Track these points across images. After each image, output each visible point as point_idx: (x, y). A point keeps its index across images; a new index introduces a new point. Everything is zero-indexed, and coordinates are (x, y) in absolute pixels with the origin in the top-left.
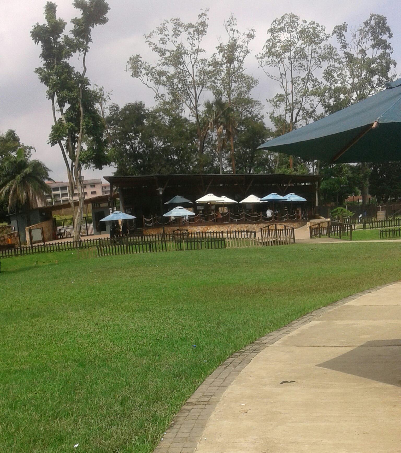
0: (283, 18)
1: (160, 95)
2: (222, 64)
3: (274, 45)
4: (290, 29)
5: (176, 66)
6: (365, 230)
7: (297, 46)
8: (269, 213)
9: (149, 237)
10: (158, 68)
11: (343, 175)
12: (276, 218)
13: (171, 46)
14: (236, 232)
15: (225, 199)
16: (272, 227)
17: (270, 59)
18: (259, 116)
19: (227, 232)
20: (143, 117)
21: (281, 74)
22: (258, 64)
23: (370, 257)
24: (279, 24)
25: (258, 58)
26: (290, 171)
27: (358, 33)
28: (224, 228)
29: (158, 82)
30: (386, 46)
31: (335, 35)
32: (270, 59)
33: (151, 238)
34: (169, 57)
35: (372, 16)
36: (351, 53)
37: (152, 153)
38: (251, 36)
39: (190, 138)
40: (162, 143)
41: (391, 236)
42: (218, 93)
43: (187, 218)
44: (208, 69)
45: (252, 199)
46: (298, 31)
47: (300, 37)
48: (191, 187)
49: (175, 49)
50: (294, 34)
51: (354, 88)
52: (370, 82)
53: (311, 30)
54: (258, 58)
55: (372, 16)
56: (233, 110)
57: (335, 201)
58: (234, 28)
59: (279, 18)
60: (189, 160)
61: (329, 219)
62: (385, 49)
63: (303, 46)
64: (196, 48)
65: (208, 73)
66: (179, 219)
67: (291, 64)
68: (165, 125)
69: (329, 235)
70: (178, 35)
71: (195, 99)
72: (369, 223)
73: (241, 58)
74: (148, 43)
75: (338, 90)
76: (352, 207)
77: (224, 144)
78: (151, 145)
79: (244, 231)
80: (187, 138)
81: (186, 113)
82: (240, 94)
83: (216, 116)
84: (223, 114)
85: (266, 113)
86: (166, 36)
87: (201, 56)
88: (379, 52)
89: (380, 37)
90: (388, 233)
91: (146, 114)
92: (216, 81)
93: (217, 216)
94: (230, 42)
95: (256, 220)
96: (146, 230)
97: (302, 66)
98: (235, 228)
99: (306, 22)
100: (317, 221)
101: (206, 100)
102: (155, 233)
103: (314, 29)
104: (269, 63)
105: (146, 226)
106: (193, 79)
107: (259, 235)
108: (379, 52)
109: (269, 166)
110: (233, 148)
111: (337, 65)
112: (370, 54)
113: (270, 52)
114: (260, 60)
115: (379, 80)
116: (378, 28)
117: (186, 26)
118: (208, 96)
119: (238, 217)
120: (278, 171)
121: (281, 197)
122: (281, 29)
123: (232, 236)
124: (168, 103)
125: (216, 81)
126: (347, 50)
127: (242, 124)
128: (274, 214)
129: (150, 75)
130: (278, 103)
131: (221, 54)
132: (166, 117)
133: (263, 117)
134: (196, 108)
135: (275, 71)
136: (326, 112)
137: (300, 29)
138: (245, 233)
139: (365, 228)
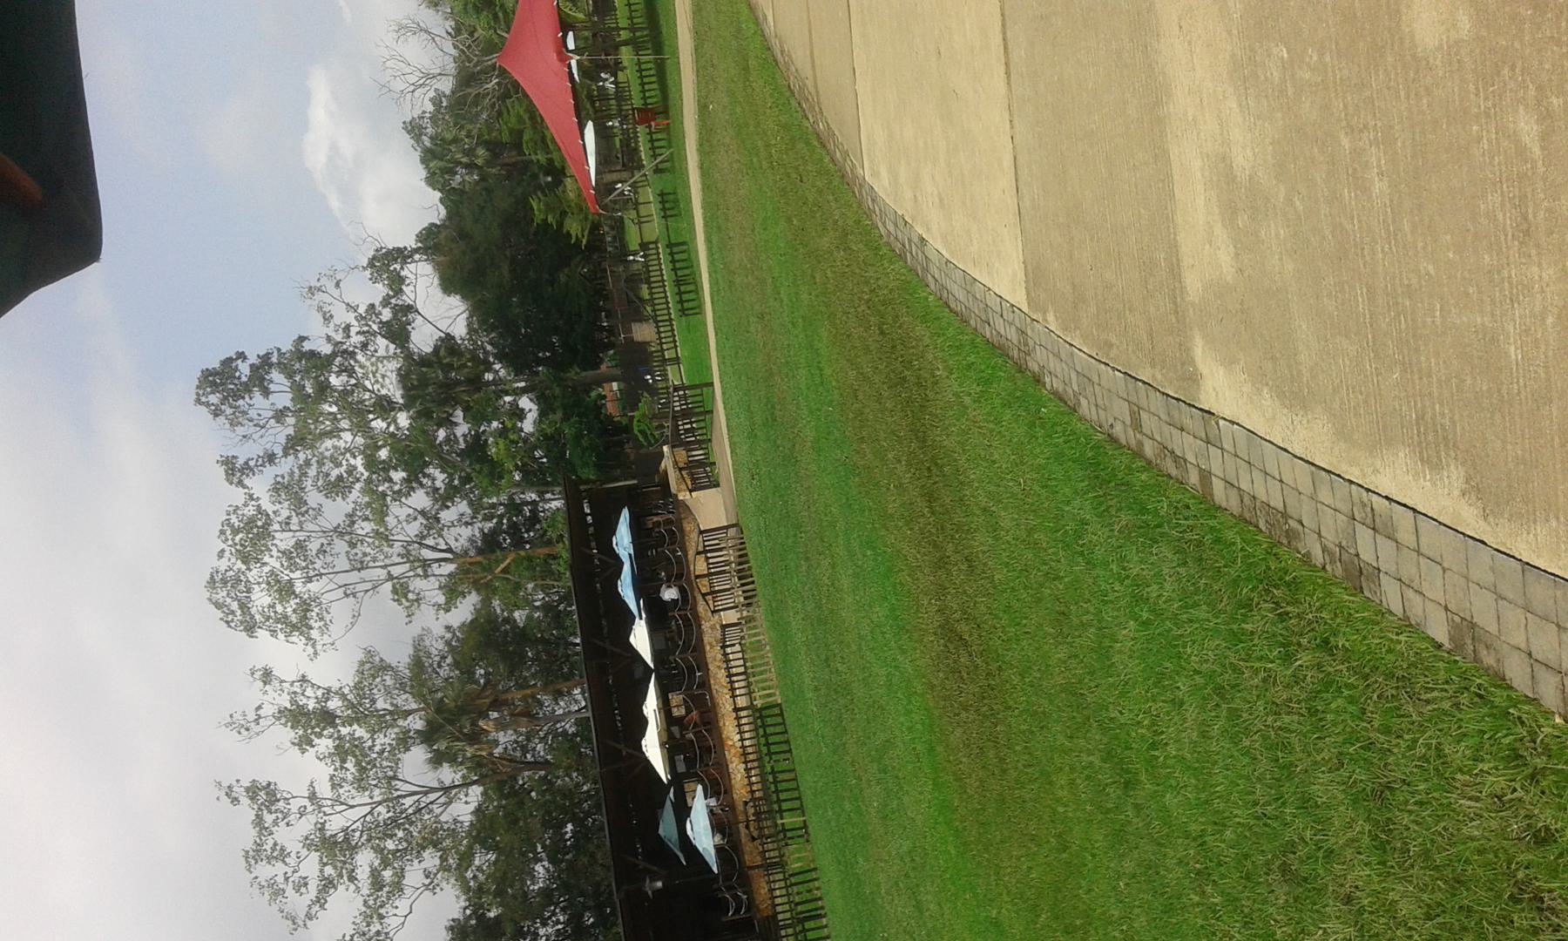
0: (218, 605)
1: (427, 881)
2: (339, 738)
3: (284, 619)
4: (242, 587)
5: (354, 849)
6: (682, 359)
7: (278, 565)
8: (669, 594)
9: (779, 909)
10: (365, 891)
11: (559, 432)
12: (680, 576)
13: (311, 866)
14: (730, 676)
15: (651, 705)
16: (704, 585)
17: (316, 625)
18: (449, 636)
19: (734, 697)
20: (481, 918)
21: (347, 596)
22: (331, 652)
23: (761, 317)
24: (233, 613)
25: (316, 653)
26: (563, 550)
27: (240, 430)
28: (725, 705)
29: (398, 887)
30: (265, 362)
31: (247, 481)
32: (316, 625)
33: (778, 893)
34: (335, 868)
35: (198, 401)
36: (284, 441)
37: (565, 887)
38: (267, 676)
39: (519, 795)
40: (539, 868)
41: (691, 287)
42: (404, 742)
43: (713, 802)
44: (353, 770)
45: (640, 639)
46: (244, 567)
47: (258, 560)
48: (634, 799)
49: (315, 856)
50: (253, 575)
51: (362, 427)
52: (345, 393)
53: (237, 539)
54: (316, 653)
55: (198, 401)
56: (441, 700)
57: (621, 444)
58: (252, 716)
59: (220, 614)
60: (568, 794)
61: (665, 448)
62: (271, 365)
63: (274, 553)
64: (306, 802)
65: (362, 770)
66: (719, 824)
67: (321, 575)
68: (495, 863)
69: (705, 443)
70: (283, 849)
71: (426, 793)
72: (662, 350)
73: (319, 693)
74: (309, 923)
75: (371, 463)
76: (630, 400)
77: (521, 714)
78: (546, 893)
79: (725, 655)
80: (521, 804)
81: (464, 809)
82: (402, 687)
83: (458, 739)
84: (451, 722)
85: (442, 619)
86: (287, 879)
87: (324, 790)
88: (278, 379)
89: (244, 379)
90: (685, 297)
91: (474, 912)
92: (377, 749)
93: (696, 725)
94: (285, 725)
95: (692, 624)
96: (759, 910)
97: (322, 551)
98: (718, 676)
99: (223, 551)
100: (673, 476)
101: (427, 767)
102: (764, 884)
103: (236, 531)
104: (324, 629)
105: (748, 910)
106: (380, 803)
107: (731, 617)
108: (278, 379)
109: (560, 602)
110: (528, 692)
111: (312, 472)
112: (284, 399)
113: (299, 625)
114: (319, 647)
115: (338, 374)
116: (225, 385)
117: (260, 834)
118: (415, 765)
119: (692, 671)
120: (567, 580)
121: (627, 568)
122: (244, 607)
123: (742, 684)
124: (443, 859)
125: (377, 749)
126: (278, 451)
127: (468, 674)
128: (668, 581)
129: (382, 911)
130: (410, 596)
131: (316, 741)
132: (477, 862)
133: (448, 628)
134: (446, 790)
135: (340, 611)
136: (422, 485)
137: (240, 565)
138: (729, 650)
139: (677, 360)
